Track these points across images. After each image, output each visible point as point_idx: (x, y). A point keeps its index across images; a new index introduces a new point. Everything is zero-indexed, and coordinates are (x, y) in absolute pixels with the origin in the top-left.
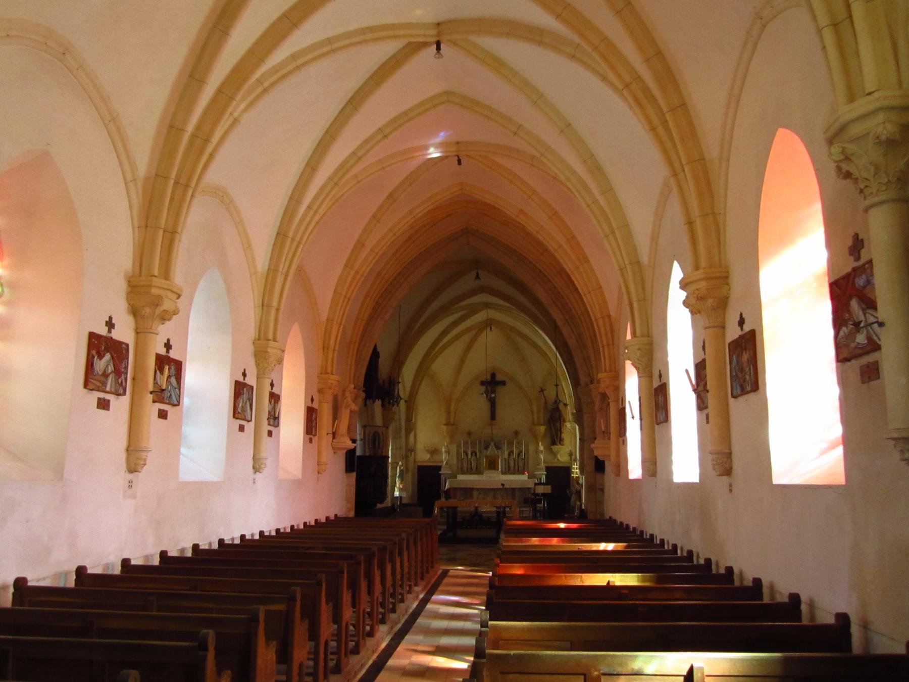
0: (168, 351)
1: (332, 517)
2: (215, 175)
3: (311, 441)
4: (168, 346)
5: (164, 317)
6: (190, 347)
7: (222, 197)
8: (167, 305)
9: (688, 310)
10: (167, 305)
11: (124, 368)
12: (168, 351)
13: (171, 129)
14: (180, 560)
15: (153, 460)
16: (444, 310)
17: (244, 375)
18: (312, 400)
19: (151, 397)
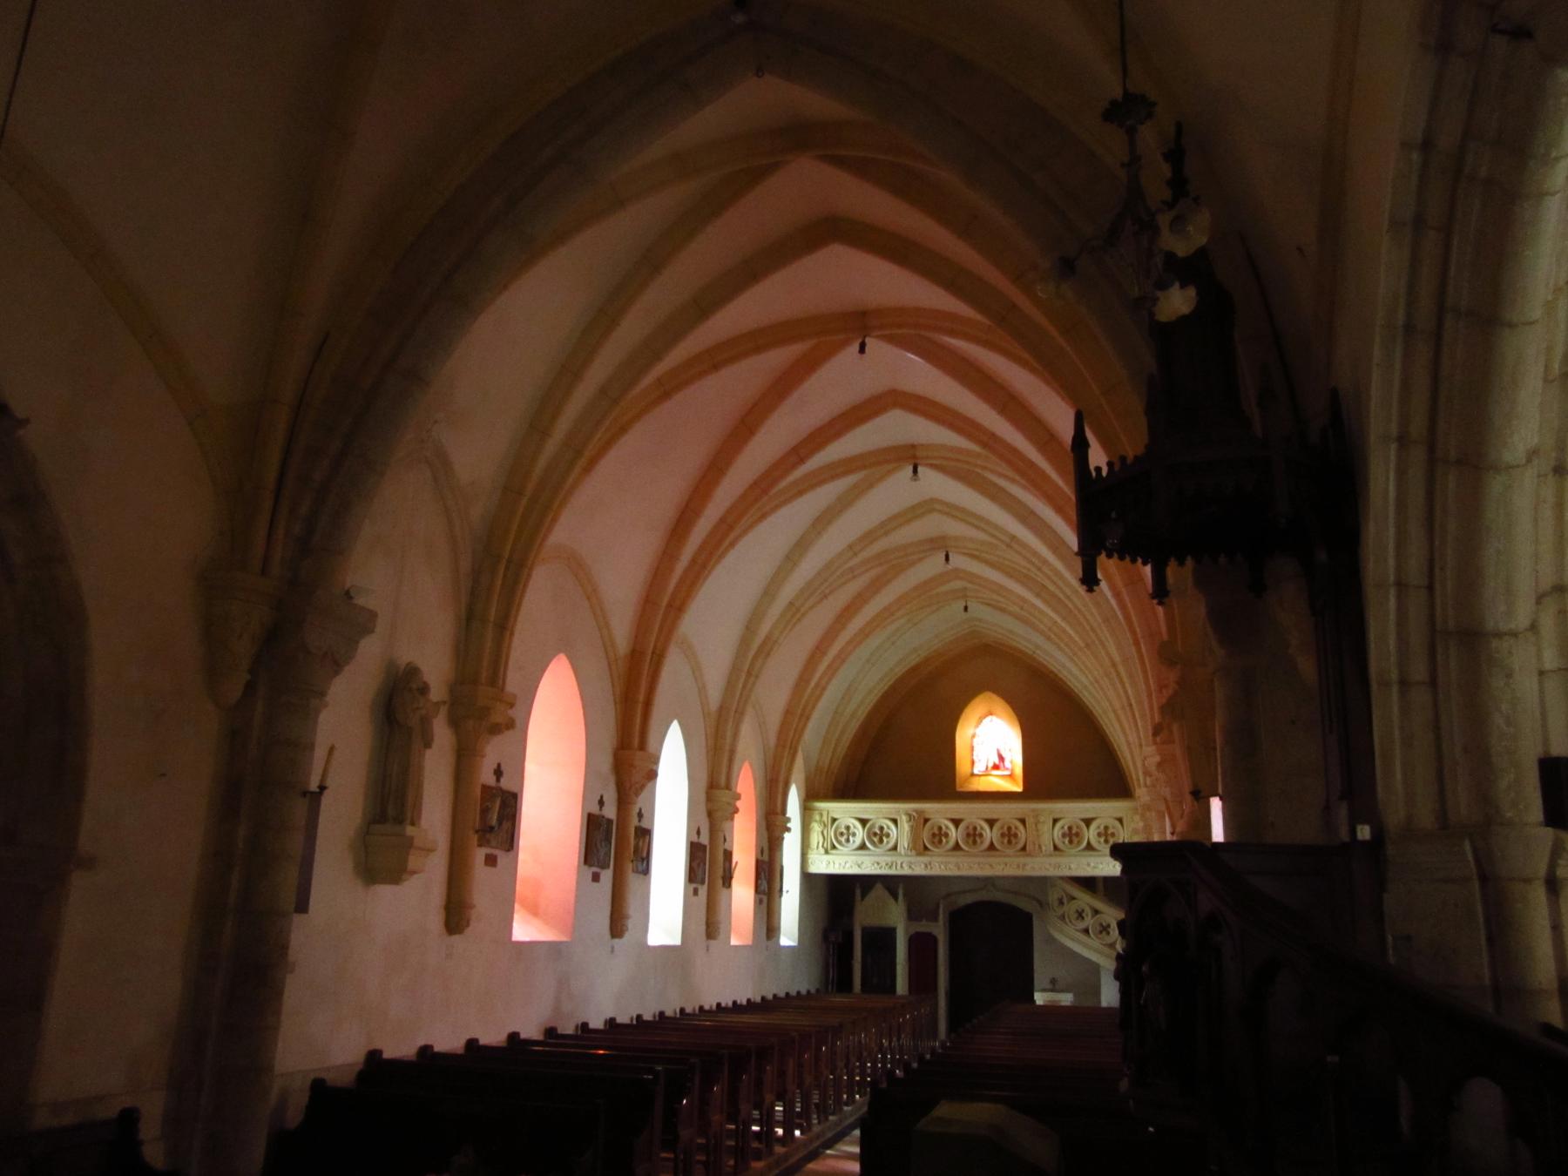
0: (498, 780)
1: (770, 997)
2: (563, 533)
3: (696, 892)
4: (498, 773)
5: (496, 730)
6: (531, 767)
7: (578, 568)
8: (496, 718)
9: (1117, 984)
10: (496, 718)
11: (1054, 986)
12: (498, 780)
13: (648, 601)
14: (397, 1067)
15: (478, 925)
16: (763, 495)
17: (601, 803)
18: (698, 833)
19: (475, 838)
